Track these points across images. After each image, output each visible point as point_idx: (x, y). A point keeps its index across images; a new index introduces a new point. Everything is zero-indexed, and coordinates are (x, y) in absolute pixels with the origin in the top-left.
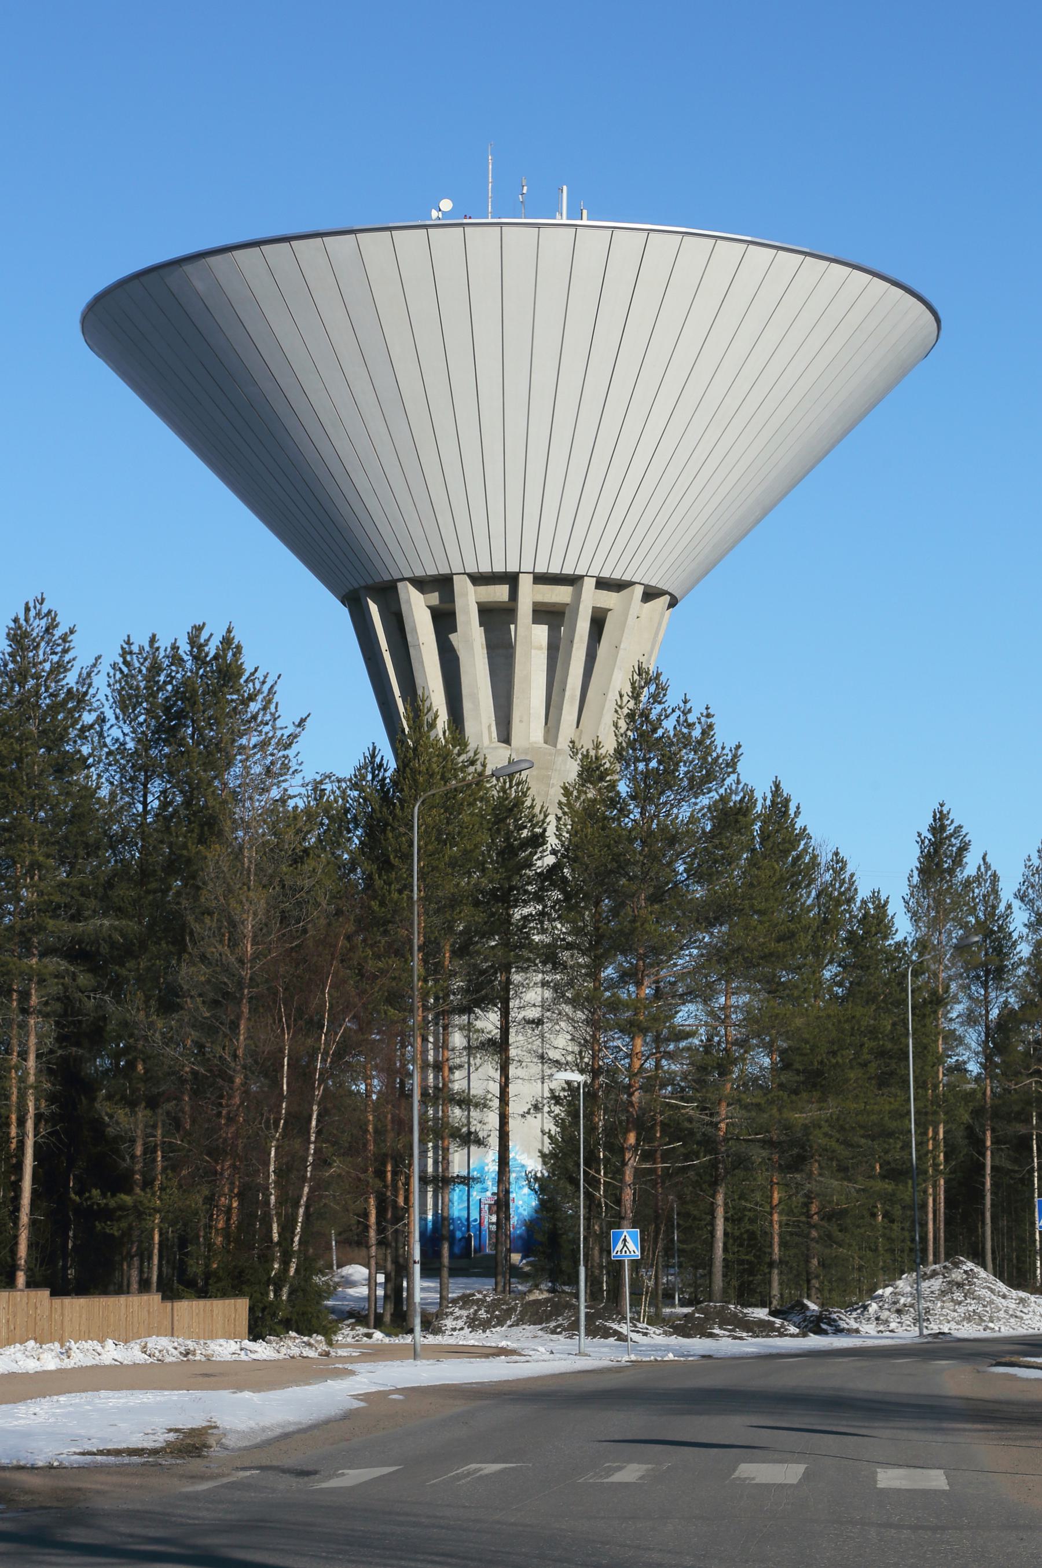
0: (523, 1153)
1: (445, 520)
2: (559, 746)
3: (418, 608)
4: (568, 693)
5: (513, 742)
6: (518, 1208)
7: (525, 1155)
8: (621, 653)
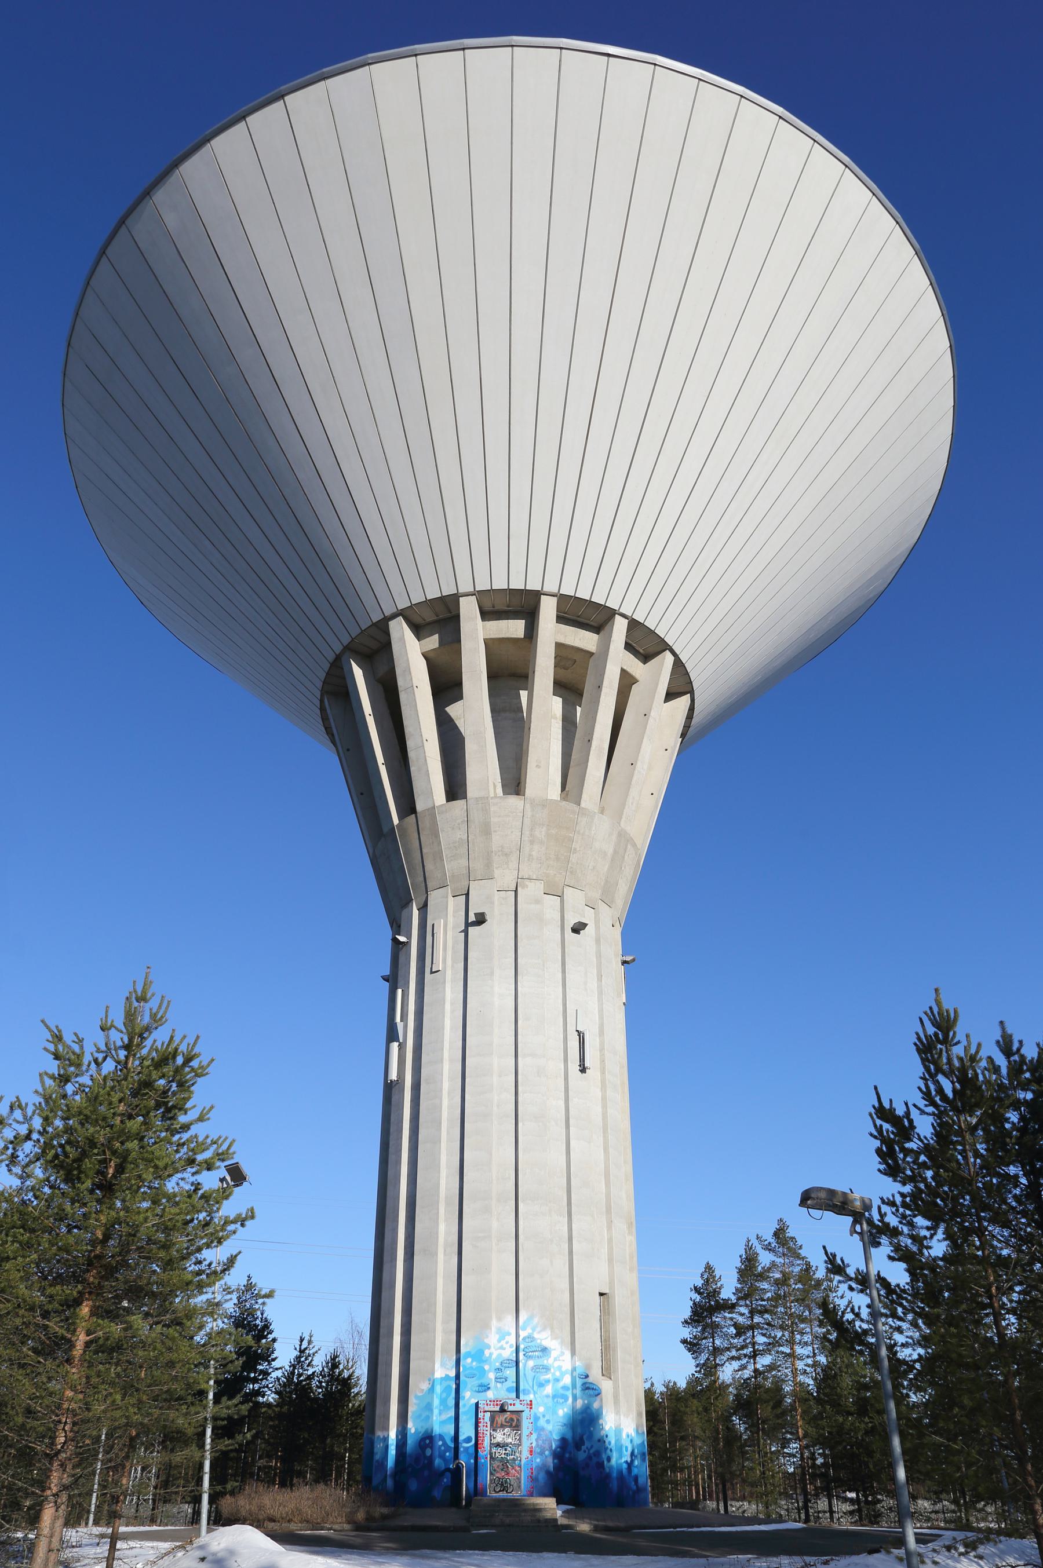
0: (544, 1329)
1: (455, 513)
2: (583, 805)
3: (412, 655)
4: (594, 743)
5: (528, 792)
6: (537, 1419)
7: (547, 1334)
8: (651, 721)
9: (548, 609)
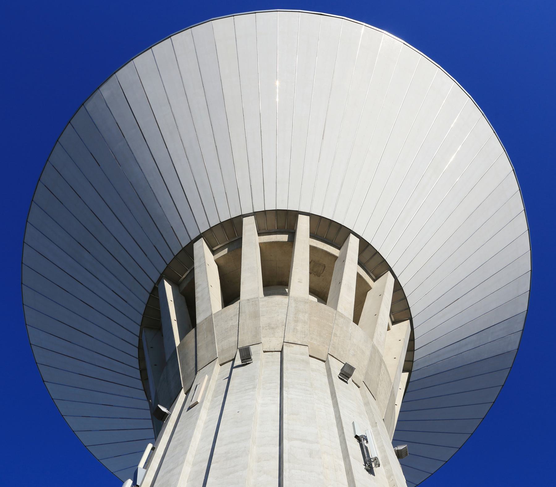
9: (303, 225)
